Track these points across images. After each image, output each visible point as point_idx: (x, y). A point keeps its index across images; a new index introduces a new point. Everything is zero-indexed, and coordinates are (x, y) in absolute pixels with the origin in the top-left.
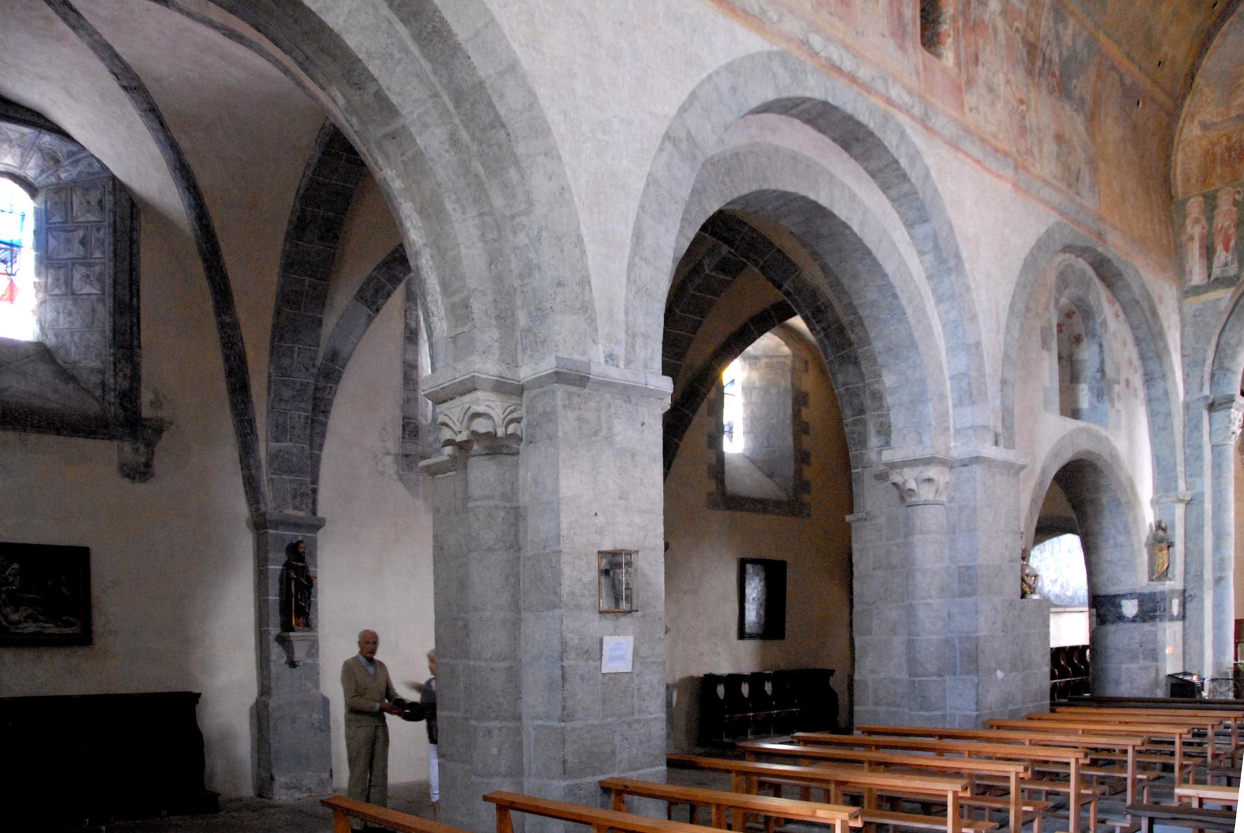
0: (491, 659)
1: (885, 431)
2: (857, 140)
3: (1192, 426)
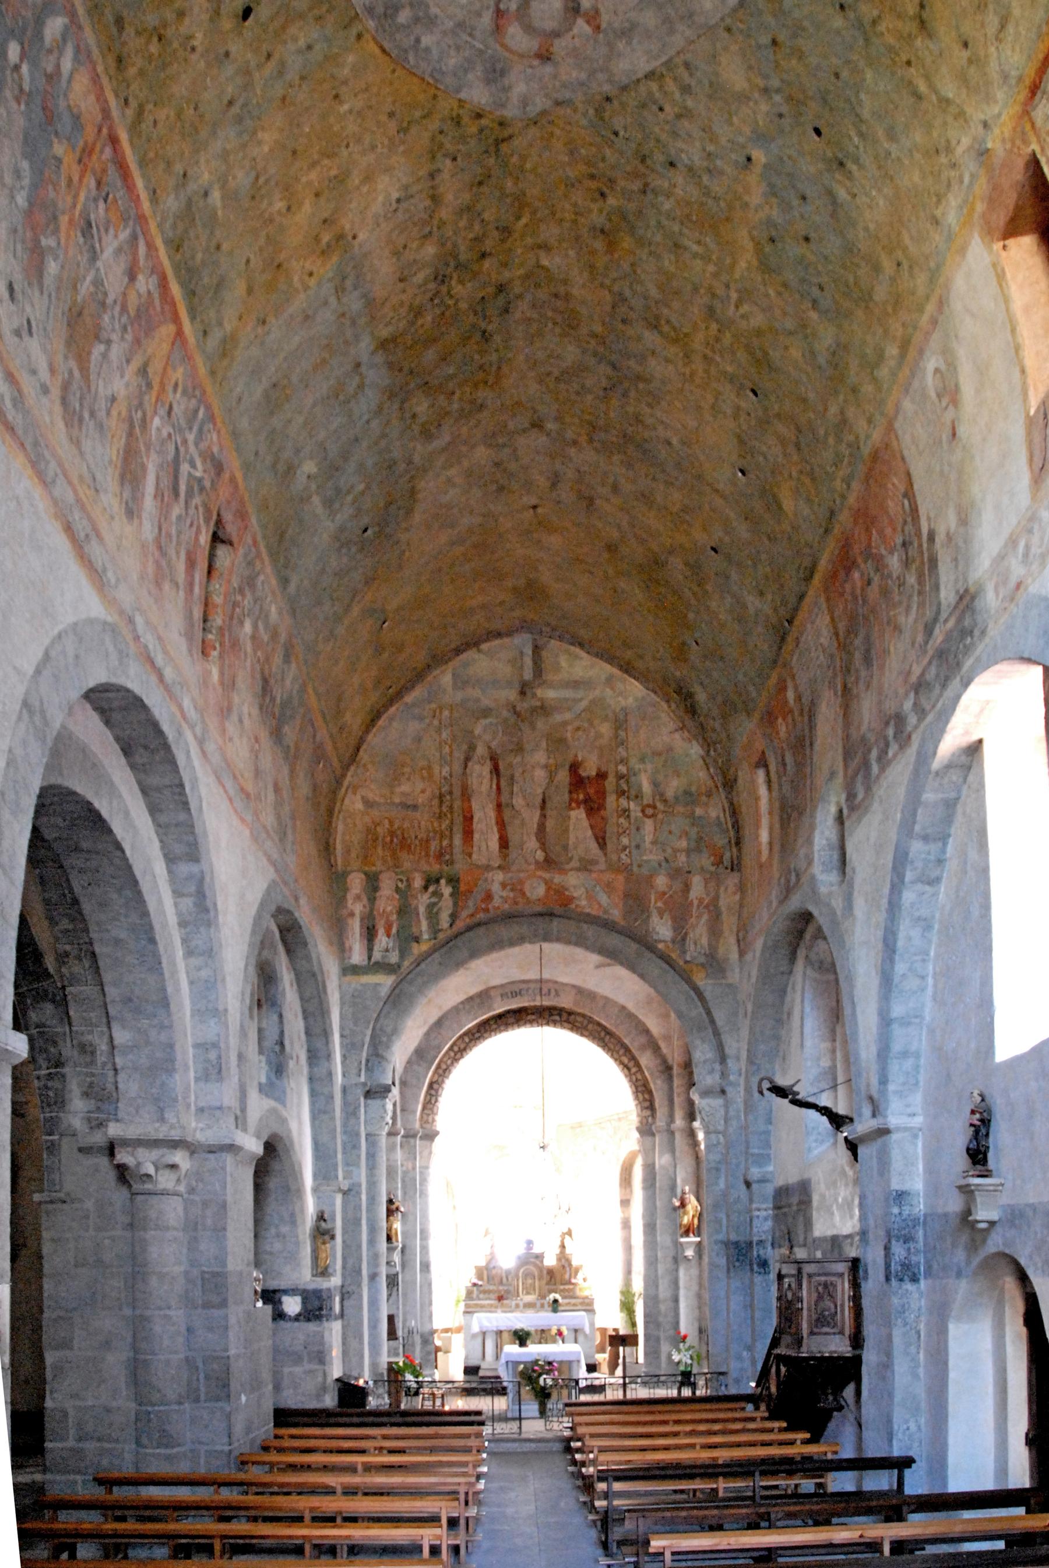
3: (351, 1112)
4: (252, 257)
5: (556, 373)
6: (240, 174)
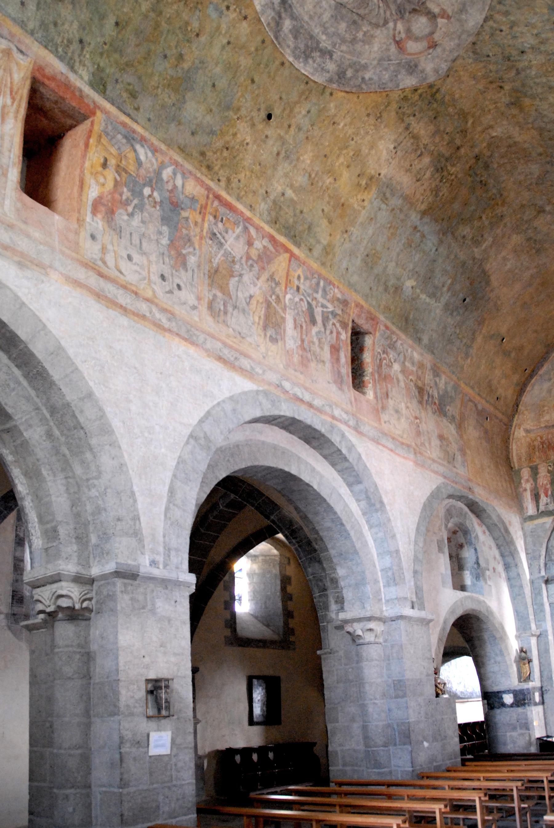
0: (69, 748)
1: (340, 601)
2: (314, 438)
3: (536, 593)
4: (324, 208)
5: (534, 181)
6: (300, 179)
